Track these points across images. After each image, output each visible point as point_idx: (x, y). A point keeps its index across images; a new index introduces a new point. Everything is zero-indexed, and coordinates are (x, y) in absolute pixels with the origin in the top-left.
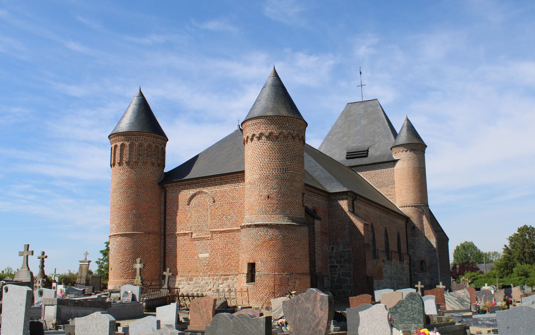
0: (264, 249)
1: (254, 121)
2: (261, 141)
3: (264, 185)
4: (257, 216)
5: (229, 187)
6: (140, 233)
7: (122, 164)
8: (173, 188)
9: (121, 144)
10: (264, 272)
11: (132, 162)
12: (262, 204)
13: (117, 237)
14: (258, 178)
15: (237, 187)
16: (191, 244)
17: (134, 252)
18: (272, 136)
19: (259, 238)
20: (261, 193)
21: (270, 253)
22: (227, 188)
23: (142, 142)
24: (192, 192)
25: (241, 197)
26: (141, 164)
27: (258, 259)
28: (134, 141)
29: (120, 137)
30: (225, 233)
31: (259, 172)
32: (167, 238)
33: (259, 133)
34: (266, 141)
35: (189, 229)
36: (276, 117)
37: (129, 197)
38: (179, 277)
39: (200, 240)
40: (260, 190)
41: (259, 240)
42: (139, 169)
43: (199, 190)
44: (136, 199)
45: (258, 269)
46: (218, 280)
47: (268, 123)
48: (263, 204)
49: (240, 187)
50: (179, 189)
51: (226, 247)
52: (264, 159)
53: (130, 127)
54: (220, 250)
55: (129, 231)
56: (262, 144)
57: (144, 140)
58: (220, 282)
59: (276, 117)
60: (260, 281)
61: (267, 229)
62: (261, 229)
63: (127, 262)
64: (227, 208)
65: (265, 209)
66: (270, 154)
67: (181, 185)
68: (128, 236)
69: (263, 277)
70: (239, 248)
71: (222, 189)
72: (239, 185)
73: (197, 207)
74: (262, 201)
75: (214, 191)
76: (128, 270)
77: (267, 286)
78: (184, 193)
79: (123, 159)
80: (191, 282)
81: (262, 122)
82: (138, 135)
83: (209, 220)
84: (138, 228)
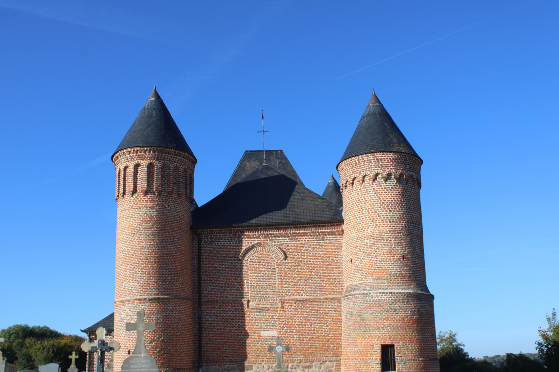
4: (389, 281)
5: (308, 241)
8: (214, 236)
10: (408, 357)
11: (164, 192)
12: (395, 266)
14: (387, 231)
15: (322, 241)
19: (398, 311)
22: (305, 241)
23: (177, 164)
25: (328, 255)
26: (176, 196)
27: (399, 339)
28: (168, 162)
31: (388, 223)
32: (203, 308)
33: (386, 173)
34: (395, 184)
40: (392, 247)
42: (173, 204)
44: (171, 247)
46: (295, 368)
48: (397, 266)
49: (325, 241)
50: (224, 237)
51: (306, 323)
52: (394, 207)
54: (297, 327)
57: (180, 163)
59: (407, 155)
60: (404, 369)
65: (400, 273)
67: (228, 232)
69: (409, 364)
71: (297, 242)
72: (325, 239)
73: (257, 264)
75: (284, 244)
82: (173, 153)
83: (277, 284)
84: (175, 290)
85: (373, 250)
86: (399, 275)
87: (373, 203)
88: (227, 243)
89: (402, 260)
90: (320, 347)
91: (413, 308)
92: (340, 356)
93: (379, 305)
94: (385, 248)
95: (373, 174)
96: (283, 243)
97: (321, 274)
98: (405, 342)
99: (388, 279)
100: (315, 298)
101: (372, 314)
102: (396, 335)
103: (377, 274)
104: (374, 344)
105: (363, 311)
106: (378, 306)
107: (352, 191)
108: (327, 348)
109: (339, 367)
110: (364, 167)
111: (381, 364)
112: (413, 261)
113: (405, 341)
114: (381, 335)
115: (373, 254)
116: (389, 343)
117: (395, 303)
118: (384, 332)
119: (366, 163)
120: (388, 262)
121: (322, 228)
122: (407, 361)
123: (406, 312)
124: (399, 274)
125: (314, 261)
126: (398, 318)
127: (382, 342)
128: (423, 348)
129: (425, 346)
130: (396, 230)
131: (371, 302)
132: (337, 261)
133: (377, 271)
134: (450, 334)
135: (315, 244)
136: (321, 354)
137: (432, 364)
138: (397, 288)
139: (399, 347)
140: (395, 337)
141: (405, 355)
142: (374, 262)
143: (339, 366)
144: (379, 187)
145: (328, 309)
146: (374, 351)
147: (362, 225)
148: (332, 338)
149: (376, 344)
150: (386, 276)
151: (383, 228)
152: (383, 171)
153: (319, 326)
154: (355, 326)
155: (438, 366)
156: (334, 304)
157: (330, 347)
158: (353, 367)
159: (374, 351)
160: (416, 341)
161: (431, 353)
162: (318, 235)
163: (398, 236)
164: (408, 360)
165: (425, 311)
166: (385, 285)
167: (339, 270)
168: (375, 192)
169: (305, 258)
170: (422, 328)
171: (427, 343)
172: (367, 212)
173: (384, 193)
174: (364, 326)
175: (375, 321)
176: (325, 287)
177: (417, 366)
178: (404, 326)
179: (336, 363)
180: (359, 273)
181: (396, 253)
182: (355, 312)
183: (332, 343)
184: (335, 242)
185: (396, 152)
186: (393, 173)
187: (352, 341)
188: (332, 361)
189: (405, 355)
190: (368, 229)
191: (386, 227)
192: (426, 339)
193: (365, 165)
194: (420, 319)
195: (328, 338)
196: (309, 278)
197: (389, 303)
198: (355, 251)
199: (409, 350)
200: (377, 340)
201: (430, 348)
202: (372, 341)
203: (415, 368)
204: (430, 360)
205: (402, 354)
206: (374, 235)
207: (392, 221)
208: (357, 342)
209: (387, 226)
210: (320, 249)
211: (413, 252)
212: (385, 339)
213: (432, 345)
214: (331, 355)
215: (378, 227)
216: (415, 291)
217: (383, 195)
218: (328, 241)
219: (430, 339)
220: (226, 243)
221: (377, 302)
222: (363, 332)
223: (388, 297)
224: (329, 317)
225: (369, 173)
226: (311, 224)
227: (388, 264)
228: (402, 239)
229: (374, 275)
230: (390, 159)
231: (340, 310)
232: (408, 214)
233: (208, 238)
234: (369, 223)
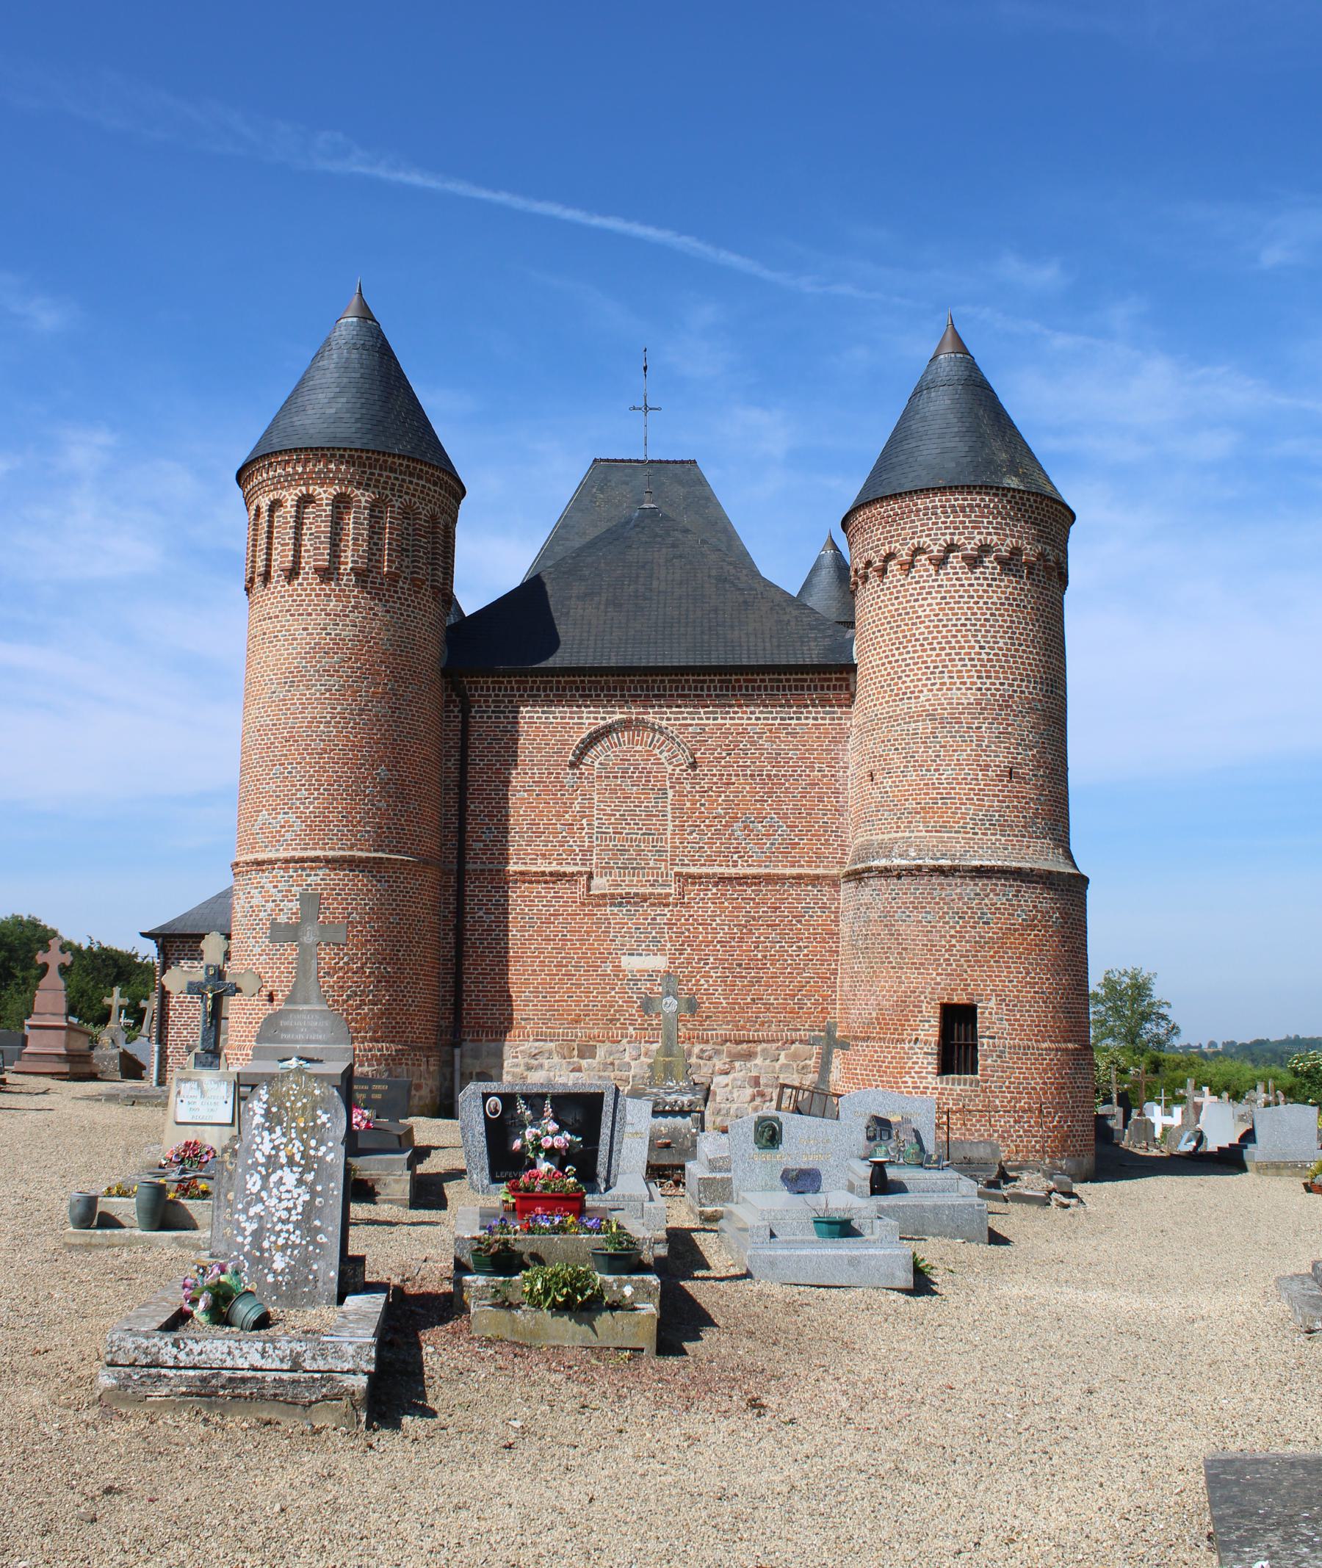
0: (1009, 957)
1: (956, 500)
2: (981, 573)
3: (996, 728)
4: (970, 835)
5: (758, 719)
6: (403, 860)
7: (335, 576)
9: (335, 496)
12: (988, 796)
13: (312, 868)
15: (794, 722)
16: (585, 915)
17: (382, 936)
18: (1017, 560)
20: (984, 758)
21: (1028, 973)
22: (749, 719)
23: (413, 499)
24: (590, 718)
28: (388, 492)
29: (343, 467)
30: (740, 885)
31: (975, 679)
34: (998, 574)
35: (578, 858)
36: (1032, 499)
37: (363, 710)
38: (531, 1038)
39: (628, 903)
41: (987, 923)
43: (621, 713)
45: (988, 1028)
46: (710, 1058)
47: (1008, 514)
48: (993, 796)
52: (992, 637)
53: (364, 431)
55: (362, 850)
56: (985, 582)
58: (719, 1063)
61: (1017, 886)
62: (996, 885)
63: (356, 973)
64: (748, 792)
66: (1012, 622)
68: (358, 866)
70: (801, 944)
71: (728, 721)
73: (616, 777)
74: (989, 785)
75: (691, 725)
76: (359, 1007)
77: (1024, 1088)
78: (552, 720)
79: (340, 557)
80: (584, 1063)
81: (987, 506)
83: (669, 832)
86: (997, 820)
87: (936, 623)
88: (539, 718)
95: (941, 545)
96: (689, 722)
101: (921, 922)
107: (882, 590)
110: (917, 527)
111: (938, 1054)
122: (1007, 1050)
133: (938, 808)
144: (954, 582)
147: (904, 682)
151: (959, 692)
152: (965, 538)
168: (943, 594)
169: (748, 764)
172: (918, 648)
173: (966, 599)
175: (929, 940)
180: (890, 811)
193: (919, 520)
195: (800, 982)
196: (755, 818)
207: (984, 674)
214: (807, 1027)
215: (948, 689)
217: (965, 603)
218: (811, 721)
220: (536, 715)
225: (929, 542)
233: (488, 701)
234: (924, 677)
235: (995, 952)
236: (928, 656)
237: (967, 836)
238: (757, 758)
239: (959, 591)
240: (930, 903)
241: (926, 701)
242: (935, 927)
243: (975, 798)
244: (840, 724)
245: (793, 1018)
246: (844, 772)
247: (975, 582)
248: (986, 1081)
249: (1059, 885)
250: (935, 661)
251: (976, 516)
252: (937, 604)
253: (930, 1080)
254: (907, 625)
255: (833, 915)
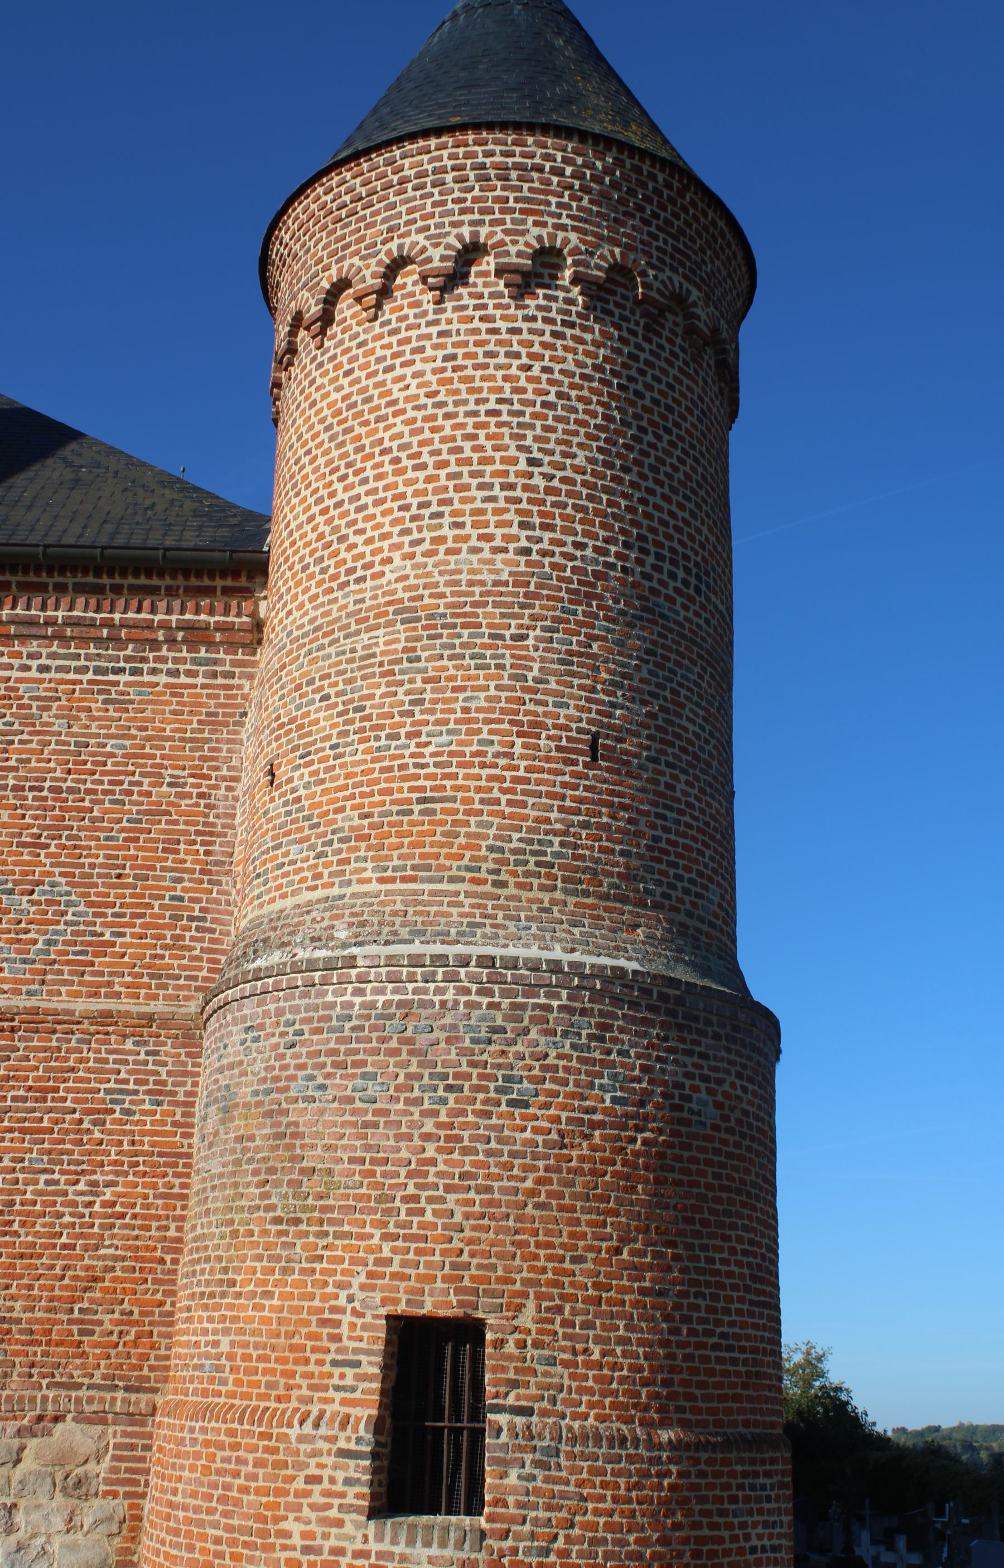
3: (561, 642)
4: (488, 888)
5: (44, 669)
10: (575, 1417)
14: (505, 576)
15: (123, 678)
19: (526, 1084)
20: (530, 707)
25: (153, 757)
27: (518, 1286)
31: (515, 530)
33: (527, 244)
34: (579, 315)
49: (147, 678)
60: (535, 1507)
65: (562, 844)
69: (574, 1470)
85: (401, 690)
86: (556, 855)
87: (430, 411)
89: (586, 765)
90: (29, 1321)
91: (639, 1080)
92: (154, 1390)
93: (402, 1041)
94: (481, 682)
95: (448, 247)
97: (92, 866)
98: (560, 1310)
99: (483, 875)
100: (35, 1011)
101: (350, 1100)
102: (500, 1256)
103: (413, 845)
104: (342, 1311)
105: (293, 1078)
106: (394, 1044)
108: (75, 1328)
109: (143, 1459)
111: (374, 1455)
112: (657, 783)
113: (563, 1297)
114: (394, 1250)
115: (402, 714)
116: (449, 1305)
117: (509, 1035)
118: (421, 1226)
119: (410, 193)
120: (495, 766)
121: (134, 603)
122: (564, 1447)
123: (583, 1098)
124: (556, 848)
125: (64, 786)
126: (528, 1134)
127: (396, 1301)
128: (687, 1358)
129: (703, 1346)
130: (560, 579)
131: (355, 1022)
132: (201, 796)
133: (412, 824)
134: (808, 1354)
135: (83, 691)
136: (32, 1365)
137: (745, 1474)
138: (535, 937)
139: (511, 1339)
140: (493, 1267)
141: (553, 1401)
142: (403, 767)
143: (139, 1453)
144: (476, 324)
145: (111, 1085)
146: (335, 1363)
148: (119, 1265)
149: (355, 1313)
150: (468, 854)
151: (474, 558)
152: (506, 232)
153: (41, 1186)
154: (236, 1185)
155: (782, 1485)
156: (155, 1053)
157: (100, 1323)
158: (193, 1469)
159: (335, 1363)
160: (635, 1304)
161: (736, 1398)
162: (109, 639)
163: (575, 613)
164: (573, 1440)
165: (718, 1105)
166: (454, 911)
167: (207, 853)
168: (450, 350)
169: (12, 763)
170: (690, 1221)
171: (719, 1323)
172: (388, 468)
173: (502, 360)
174: (290, 1183)
175: (368, 1148)
176: (113, 944)
177: (638, 1486)
178: (561, 1196)
179: (125, 1434)
180: (301, 841)
181: (546, 714)
182: (245, 1093)
183: (112, 1302)
184: (204, 686)
185: (603, 142)
186: (571, 253)
187: (208, 1283)
188: (100, 1419)
189: (553, 1401)
190: (387, 569)
191: (499, 557)
192: (715, 1297)
194: (678, 1159)
195: (87, 1268)
196: (16, 883)
197: (470, 1029)
198: (298, 708)
199: (589, 1365)
200: (362, 1278)
201: (734, 1361)
202: (330, 1289)
203: (615, 1499)
204: (728, 1444)
205: (533, 1391)
206: (421, 598)
207: (537, 520)
208: (238, 1295)
209: (505, 550)
210: (112, 719)
211: (658, 728)
212: (421, 1278)
213: (748, 1338)
214: (97, 1380)
215: (449, 552)
216: (658, 967)
217: (499, 367)
218: (163, 679)
219: (741, 1300)
221: (391, 1017)
222: (277, 1221)
223: (467, 991)
224: (111, 1132)
226: (74, 571)
227: (491, 778)
228: (596, 638)
229: (394, 847)
230: (559, 172)
231: (188, 1094)
232: (642, 501)
234: (396, 530)
235: (539, 1181)
236: (408, 483)
237: (480, 889)
238: (32, 751)
239: (486, 342)
240: (376, 1052)
241: (397, 580)
242: (387, 1112)
243: (504, 798)
244: (230, 687)
245: (66, 1355)
246: (229, 789)
247: (525, 326)
248: (505, 1535)
249: (708, 1023)
250: (424, 492)
251: (531, 190)
252: (434, 372)
253: (349, 1528)
254: (366, 423)
255: (179, 1111)
